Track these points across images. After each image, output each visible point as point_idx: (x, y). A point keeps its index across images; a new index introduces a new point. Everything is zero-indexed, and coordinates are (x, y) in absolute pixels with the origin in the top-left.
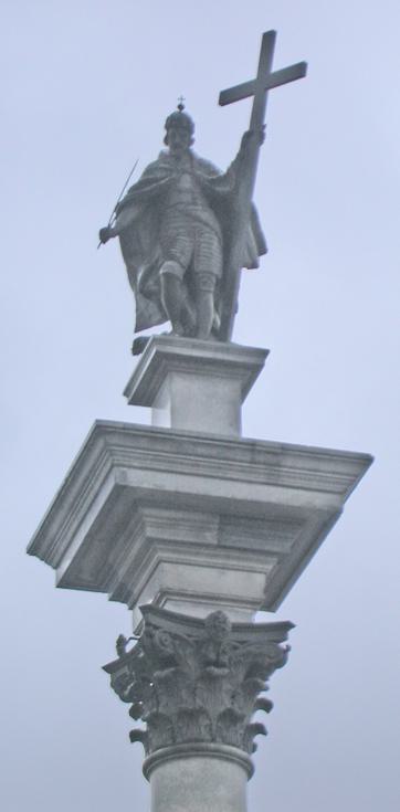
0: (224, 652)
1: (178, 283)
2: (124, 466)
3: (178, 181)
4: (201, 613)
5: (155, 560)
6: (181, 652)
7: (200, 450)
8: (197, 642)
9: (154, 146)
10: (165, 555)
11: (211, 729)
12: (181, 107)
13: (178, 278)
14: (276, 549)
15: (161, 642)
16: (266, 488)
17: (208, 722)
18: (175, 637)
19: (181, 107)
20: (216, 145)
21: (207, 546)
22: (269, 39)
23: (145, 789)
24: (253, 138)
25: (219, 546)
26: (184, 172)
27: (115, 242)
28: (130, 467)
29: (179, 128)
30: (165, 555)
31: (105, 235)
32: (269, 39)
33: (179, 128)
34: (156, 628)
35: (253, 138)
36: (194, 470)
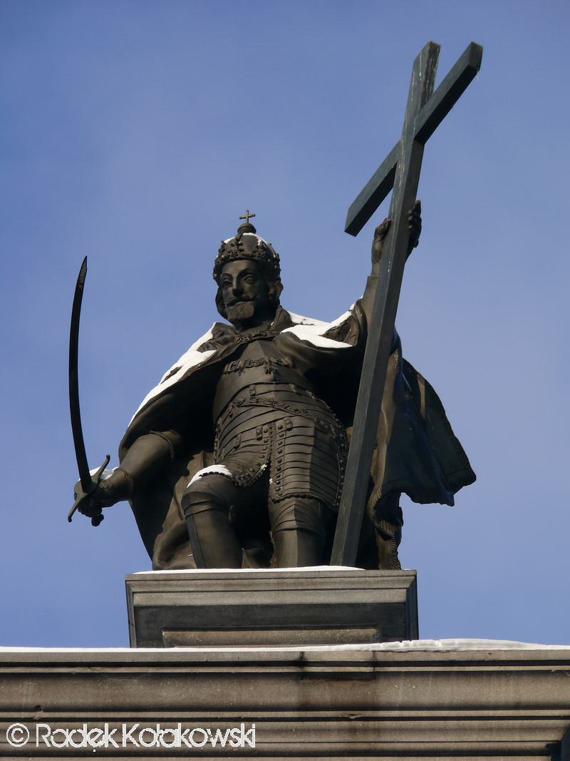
27: (121, 514)
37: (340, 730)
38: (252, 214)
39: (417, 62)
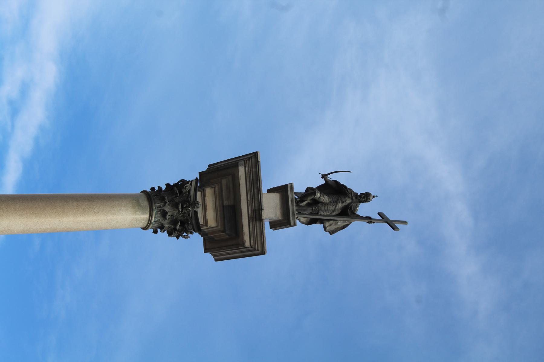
0: (186, 210)
1: (313, 197)
2: (245, 164)
3: (349, 197)
4: (199, 199)
5: (219, 226)
6: (184, 195)
7: (256, 191)
8: (189, 200)
9: (359, 190)
10: (217, 189)
11: (159, 208)
12: (374, 197)
13: (314, 197)
14: (226, 229)
15: (186, 186)
16: (247, 217)
17: (162, 206)
18: (189, 192)
19: (374, 197)
20: (363, 209)
21: (223, 202)
22: (405, 222)
23: (138, 191)
24: (369, 220)
25: (223, 206)
26: (352, 199)
27: (323, 182)
28: (245, 167)
29: (366, 197)
30: (217, 189)
31: (324, 176)
32: (405, 222)
33: (366, 197)
34: (191, 184)
35: (369, 220)
36: (252, 235)
37: (252, 216)
39: (245, 235)
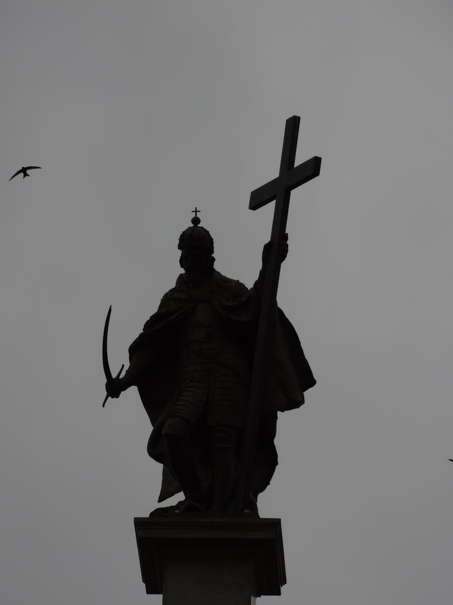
12: (196, 221)
19: (196, 221)
38: (193, 213)
